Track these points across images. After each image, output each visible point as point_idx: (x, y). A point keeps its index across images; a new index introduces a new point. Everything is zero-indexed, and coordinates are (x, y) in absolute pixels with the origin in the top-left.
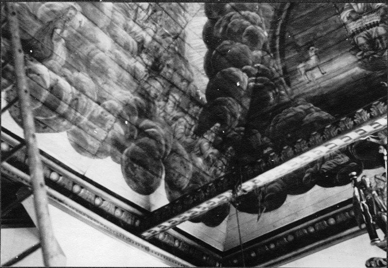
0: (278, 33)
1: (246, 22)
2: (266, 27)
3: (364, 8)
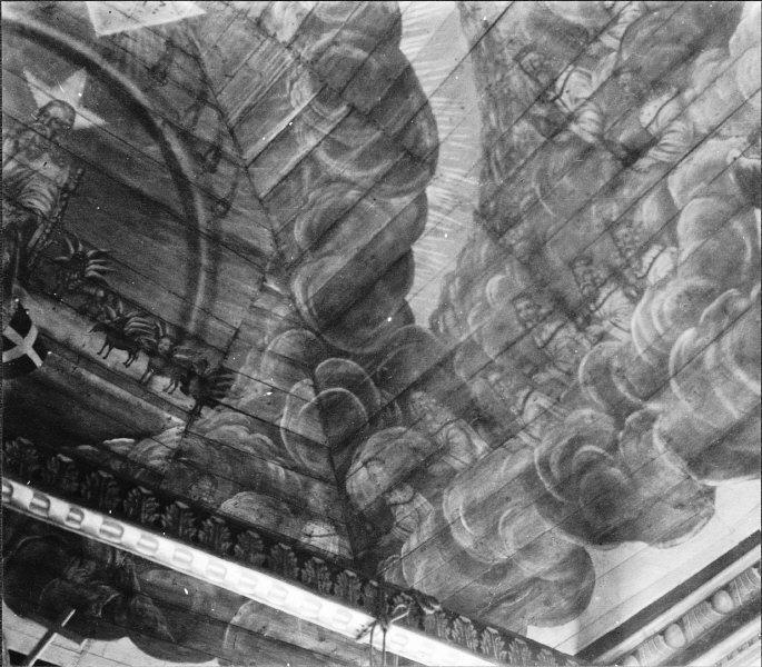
3: (11, 179)
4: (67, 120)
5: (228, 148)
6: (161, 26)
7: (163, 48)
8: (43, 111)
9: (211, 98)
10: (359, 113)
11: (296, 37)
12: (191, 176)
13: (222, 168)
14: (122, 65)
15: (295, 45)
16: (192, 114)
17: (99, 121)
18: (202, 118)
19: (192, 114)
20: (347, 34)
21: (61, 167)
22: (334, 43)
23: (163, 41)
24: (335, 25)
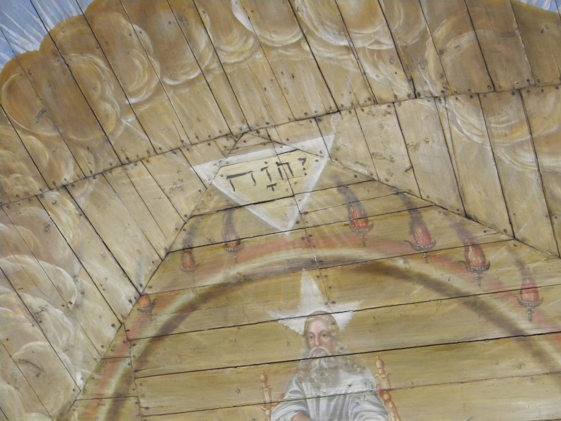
0: (110, 391)
1: (29, 327)
2: (86, 362)
4: (330, 327)
5: (479, 235)
6: (320, 179)
7: (340, 197)
8: (307, 335)
9: (418, 202)
10: (73, 186)
11: (411, 80)
12: (471, 288)
13: (492, 256)
14: (328, 243)
15: (419, 89)
16: (419, 231)
17: (355, 305)
18: (430, 228)
19: (419, 231)
20: (441, 33)
21: (361, 372)
22: (440, 53)
23: (335, 190)
24: (423, 37)
